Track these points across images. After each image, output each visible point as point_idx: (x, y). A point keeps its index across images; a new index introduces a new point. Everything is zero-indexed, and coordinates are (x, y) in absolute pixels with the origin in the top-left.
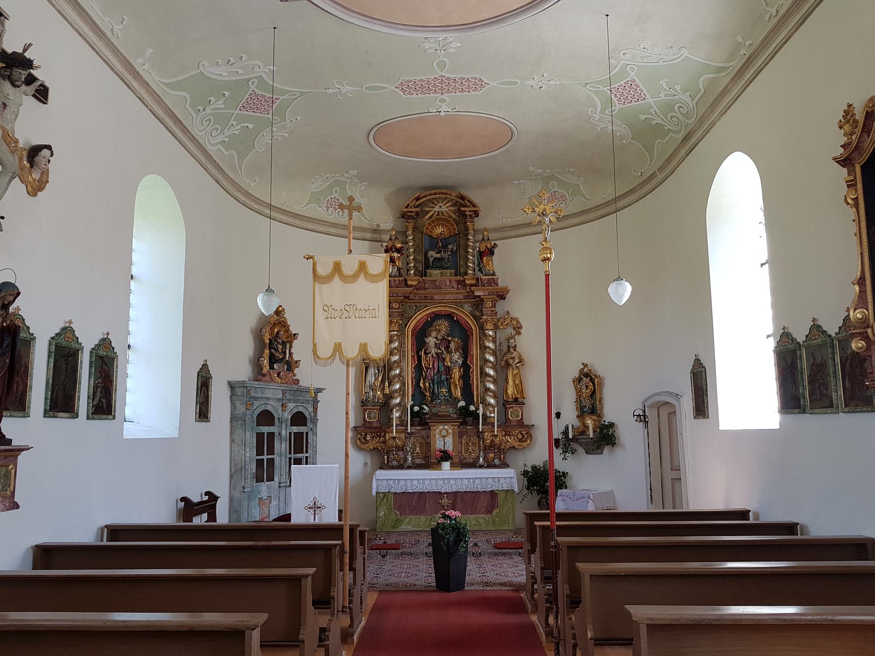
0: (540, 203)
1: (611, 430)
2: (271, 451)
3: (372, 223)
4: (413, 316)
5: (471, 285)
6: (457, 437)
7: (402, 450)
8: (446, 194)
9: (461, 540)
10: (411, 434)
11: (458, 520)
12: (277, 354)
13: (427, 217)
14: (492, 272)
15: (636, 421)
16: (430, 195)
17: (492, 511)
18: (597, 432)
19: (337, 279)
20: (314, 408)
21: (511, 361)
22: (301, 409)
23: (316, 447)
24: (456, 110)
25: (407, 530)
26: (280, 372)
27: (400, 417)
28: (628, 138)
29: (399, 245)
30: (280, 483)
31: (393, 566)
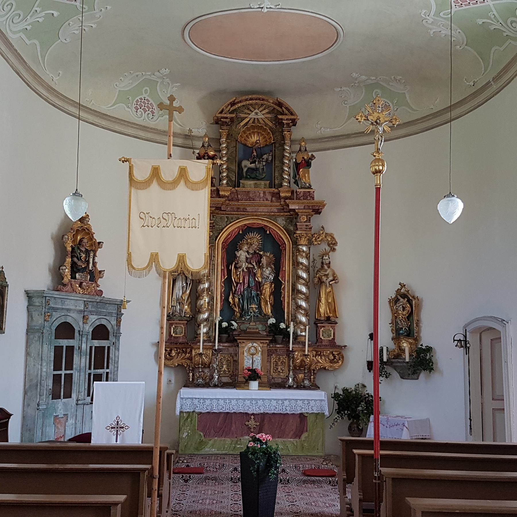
0: (374, 111)
1: (428, 354)
2: (70, 366)
3: (184, 128)
4: (224, 228)
5: (286, 198)
6: (267, 355)
7: (209, 367)
8: (263, 100)
9: (271, 466)
10: (219, 351)
11: (269, 444)
12: (79, 263)
13: (242, 124)
14: (308, 185)
15: (456, 346)
16: (246, 100)
17: (301, 436)
18: (413, 355)
19: (155, 185)
20: (117, 320)
21: (324, 278)
22: (104, 322)
23: (118, 362)
24: (280, 7)
25: (210, 453)
26: (83, 282)
27: (207, 333)
28: (463, 44)
29: (212, 153)
30: (77, 400)
31: (197, 492)
